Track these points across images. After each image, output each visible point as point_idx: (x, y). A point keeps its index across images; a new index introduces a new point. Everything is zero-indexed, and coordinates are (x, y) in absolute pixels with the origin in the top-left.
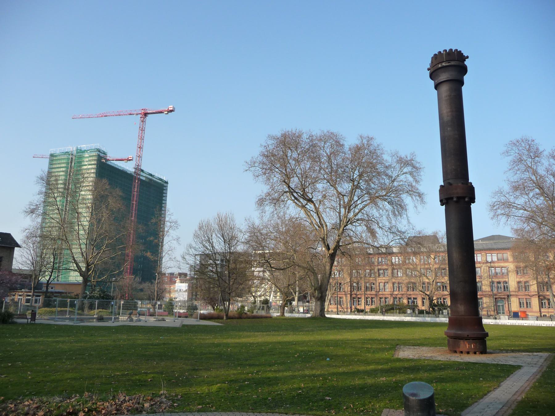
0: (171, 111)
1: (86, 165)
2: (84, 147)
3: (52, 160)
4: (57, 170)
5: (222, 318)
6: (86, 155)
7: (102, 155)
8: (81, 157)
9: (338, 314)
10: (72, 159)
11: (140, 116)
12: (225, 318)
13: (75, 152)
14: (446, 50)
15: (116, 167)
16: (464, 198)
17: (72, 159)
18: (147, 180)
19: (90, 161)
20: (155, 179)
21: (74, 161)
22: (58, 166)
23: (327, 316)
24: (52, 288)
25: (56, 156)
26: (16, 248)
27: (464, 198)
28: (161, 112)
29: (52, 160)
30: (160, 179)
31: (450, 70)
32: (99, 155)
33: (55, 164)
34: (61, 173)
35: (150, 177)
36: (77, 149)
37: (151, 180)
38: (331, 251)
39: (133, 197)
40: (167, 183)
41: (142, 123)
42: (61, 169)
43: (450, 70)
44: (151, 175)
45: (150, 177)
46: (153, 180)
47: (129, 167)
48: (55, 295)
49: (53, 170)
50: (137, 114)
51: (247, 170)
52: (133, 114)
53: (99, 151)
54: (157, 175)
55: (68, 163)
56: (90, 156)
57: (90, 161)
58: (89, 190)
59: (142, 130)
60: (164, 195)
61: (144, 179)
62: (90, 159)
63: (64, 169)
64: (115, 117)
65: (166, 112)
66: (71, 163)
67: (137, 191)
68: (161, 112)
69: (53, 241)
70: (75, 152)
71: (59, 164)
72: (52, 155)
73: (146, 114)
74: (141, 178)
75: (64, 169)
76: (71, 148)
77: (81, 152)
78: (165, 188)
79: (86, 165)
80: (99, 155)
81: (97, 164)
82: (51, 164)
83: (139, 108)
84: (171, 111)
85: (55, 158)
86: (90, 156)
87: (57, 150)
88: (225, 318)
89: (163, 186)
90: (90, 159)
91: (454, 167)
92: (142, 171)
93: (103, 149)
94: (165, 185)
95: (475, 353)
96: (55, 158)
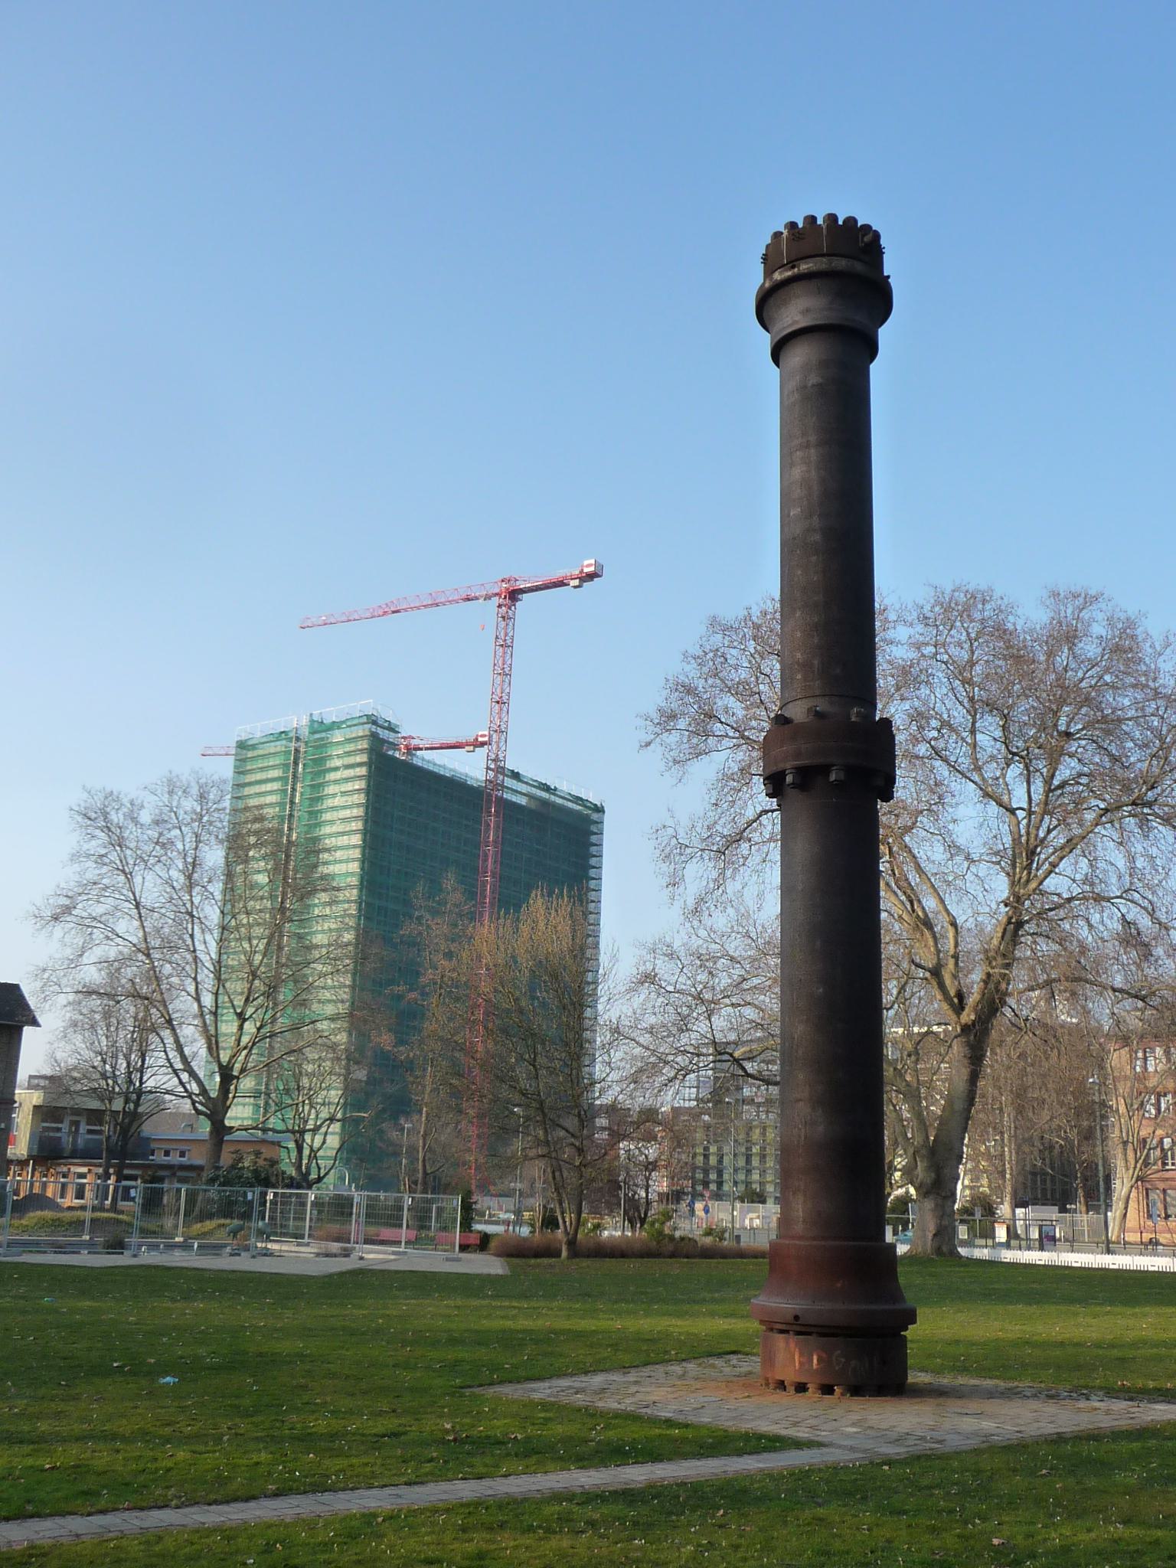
0: (591, 576)
1: (336, 769)
2: (331, 714)
3: (244, 760)
4: (257, 789)
5: (558, 1254)
6: (338, 736)
7: (384, 734)
8: (323, 745)
9: (1109, 1251)
10: (297, 751)
11: (496, 601)
12: (564, 1254)
13: (305, 733)
14: (813, 219)
15: (431, 768)
16: (825, 769)
17: (297, 751)
18: (533, 805)
19: (348, 754)
20: (560, 801)
21: (305, 755)
22: (259, 776)
23: (963, 1251)
24: (182, 1154)
25: (254, 747)
26: (26, 1029)
27: (825, 769)
28: (560, 584)
29: (244, 760)
30: (578, 800)
31: (832, 293)
32: (374, 736)
33: (250, 771)
34: (269, 799)
35: (544, 795)
36: (312, 721)
37: (545, 803)
38: (968, 1016)
39: (486, 860)
40: (600, 810)
41: (503, 624)
42: (269, 787)
43: (832, 293)
44: (546, 788)
45: (544, 795)
46: (554, 805)
47: (471, 767)
48: (179, 1174)
49: (247, 791)
50: (488, 597)
51: (648, 744)
52: (477, 598)
53: (374, 723)
54: (565, 786)
55: (286, 766)
56: (349, 740)
57: (348, 754)
58: (328, 850)
59: (505, 645)
60: (593, 849)
61: (523, 801)
62: (351, 747)
63: (276, 786)
64: (424, 611)
65: (576, 582)
66: (296, 763)
67: (495, 841)
68: (560, 584)
69: (135, 1001)
70: (305, 733)
71: (262, 769)
72: (242, 745)
73: (514, 595)
74: (514, 798)
75: (276, 786)
76: (296, 720)
77: (320, 727)
78: (593, 828)
79: (336, 769)
80: (374, 736)
81: (369, 764)
82: (239, 772)
83: (491, 577)
84: (591, 576)
85: (250, 754)
86: (349, 740)
87: (256, 728)
88: (564, 1254)
89: (587, 820)
90: (351, 747)
91: (799, 655)
92: (516, 776)
93: (387, 715)
94: (595, 816)
95: (827, 1390)
96: (250, 754)
